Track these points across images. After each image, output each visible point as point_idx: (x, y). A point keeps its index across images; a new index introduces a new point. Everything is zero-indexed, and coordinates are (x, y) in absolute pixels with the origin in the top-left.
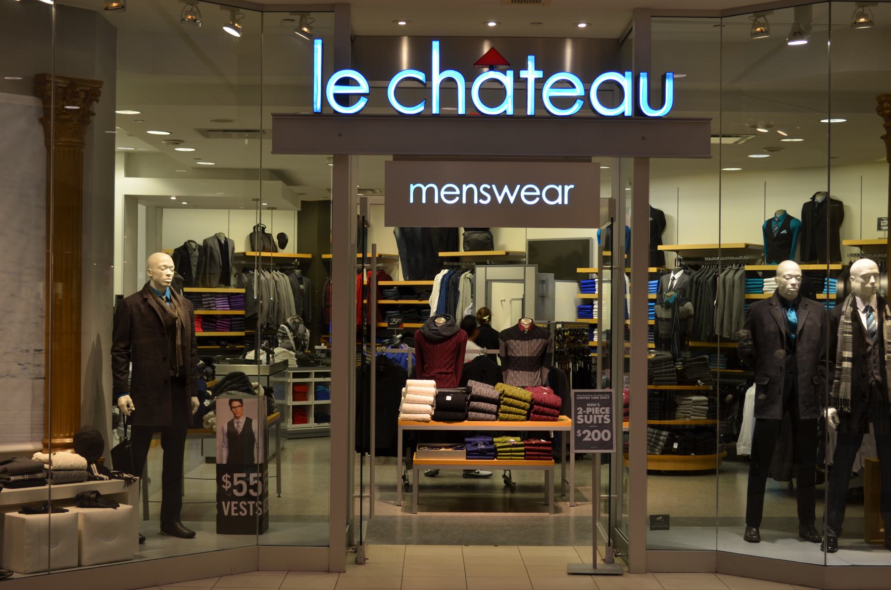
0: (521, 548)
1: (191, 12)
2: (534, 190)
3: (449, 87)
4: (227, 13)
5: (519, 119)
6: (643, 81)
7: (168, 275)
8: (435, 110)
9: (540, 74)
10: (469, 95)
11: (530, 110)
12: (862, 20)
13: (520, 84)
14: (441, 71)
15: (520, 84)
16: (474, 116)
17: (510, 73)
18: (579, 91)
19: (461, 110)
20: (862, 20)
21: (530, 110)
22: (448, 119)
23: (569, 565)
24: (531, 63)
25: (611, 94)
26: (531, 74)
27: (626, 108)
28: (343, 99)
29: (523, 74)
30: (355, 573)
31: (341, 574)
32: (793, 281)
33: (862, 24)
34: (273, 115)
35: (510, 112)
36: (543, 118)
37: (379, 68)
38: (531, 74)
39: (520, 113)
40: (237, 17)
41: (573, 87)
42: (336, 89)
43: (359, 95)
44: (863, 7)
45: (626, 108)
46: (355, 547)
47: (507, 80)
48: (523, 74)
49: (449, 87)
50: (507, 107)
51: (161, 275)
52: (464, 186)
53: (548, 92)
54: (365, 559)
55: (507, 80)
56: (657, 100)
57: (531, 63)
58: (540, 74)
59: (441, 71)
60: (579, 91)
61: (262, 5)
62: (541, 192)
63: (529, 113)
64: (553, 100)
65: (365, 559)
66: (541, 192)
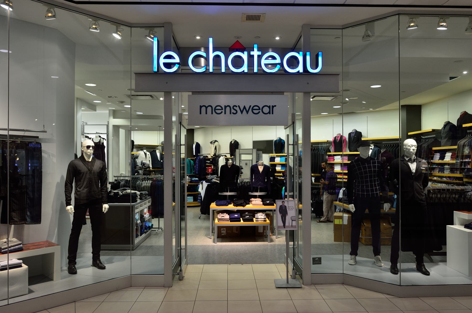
0: (254, 266)
1: (95, 25)
2: (274, 58)
3: (217, 58)
4: (114, 27)
5: (250, 73)
6: (308, 58)
7: (414, 150)
8: (211, 70)
9: (260, 53)
10: (227, 63)
11: (256, 70)
12: (412, 24)
13: (251, 57)
14: (213, 52)
15: (251, 57)
16: (229, 73)
17: (246, 53)
18: (278, 61)
19: (223, 70)
20: (412, 24)
21: (256, 70)
22: (217, 74)
23: (275, 281)
24: (256, 49)
25: (293, 62)
26: (256, 53)
27: (300, 68)
28: (168, 65)
29: (252, 53)
30: (177, 287)
31: (170, 289)
32: (414, 148)
33: (412, 26)
34: (136, 74)
35: (246, 71)
36: (262, 73)
37: (184, 53)
38: (256, 53)
39: (251, 72)
40: (119, 29)
41: (174, 58)
42: (164, 61)
43: (174, 64)
44: (412, 18)
45: (300, 68)
46: (177, 273)
47: (245, 56)
48: (252, 53)
49: (217, 58)
50: (245, 68)
51: (410, 149)
52: (301, 71)
53: (263, 62)
54: (183, 277)
55: (245, 56)
56: (315, 65)
57: (256, 49)
58: (260, 53)
59: (213, 52)
60: (278, 61)
61: (131, 24)
62: (282, 59)
63: (255, 71)
64: (266, 65)
65: (183, 277)
66: (282, 59)
